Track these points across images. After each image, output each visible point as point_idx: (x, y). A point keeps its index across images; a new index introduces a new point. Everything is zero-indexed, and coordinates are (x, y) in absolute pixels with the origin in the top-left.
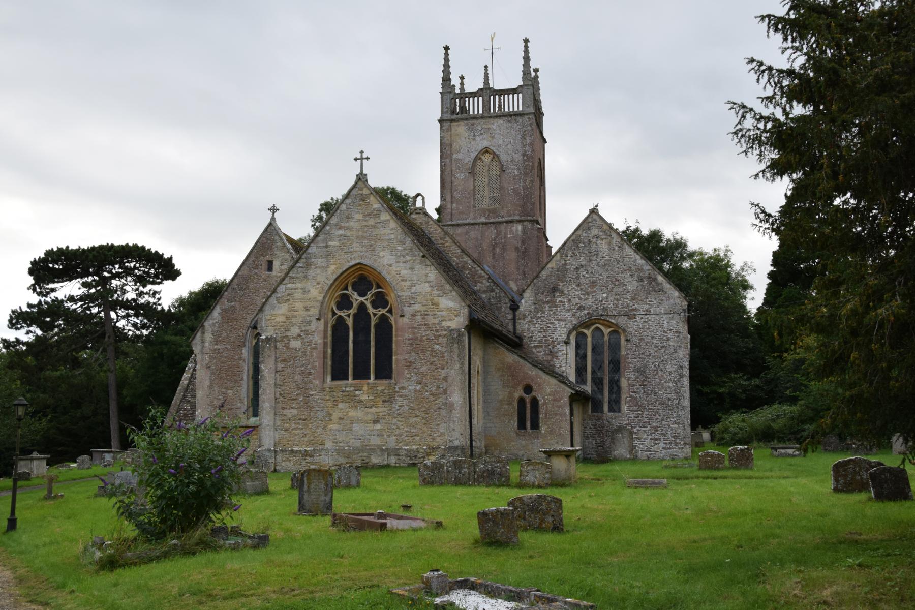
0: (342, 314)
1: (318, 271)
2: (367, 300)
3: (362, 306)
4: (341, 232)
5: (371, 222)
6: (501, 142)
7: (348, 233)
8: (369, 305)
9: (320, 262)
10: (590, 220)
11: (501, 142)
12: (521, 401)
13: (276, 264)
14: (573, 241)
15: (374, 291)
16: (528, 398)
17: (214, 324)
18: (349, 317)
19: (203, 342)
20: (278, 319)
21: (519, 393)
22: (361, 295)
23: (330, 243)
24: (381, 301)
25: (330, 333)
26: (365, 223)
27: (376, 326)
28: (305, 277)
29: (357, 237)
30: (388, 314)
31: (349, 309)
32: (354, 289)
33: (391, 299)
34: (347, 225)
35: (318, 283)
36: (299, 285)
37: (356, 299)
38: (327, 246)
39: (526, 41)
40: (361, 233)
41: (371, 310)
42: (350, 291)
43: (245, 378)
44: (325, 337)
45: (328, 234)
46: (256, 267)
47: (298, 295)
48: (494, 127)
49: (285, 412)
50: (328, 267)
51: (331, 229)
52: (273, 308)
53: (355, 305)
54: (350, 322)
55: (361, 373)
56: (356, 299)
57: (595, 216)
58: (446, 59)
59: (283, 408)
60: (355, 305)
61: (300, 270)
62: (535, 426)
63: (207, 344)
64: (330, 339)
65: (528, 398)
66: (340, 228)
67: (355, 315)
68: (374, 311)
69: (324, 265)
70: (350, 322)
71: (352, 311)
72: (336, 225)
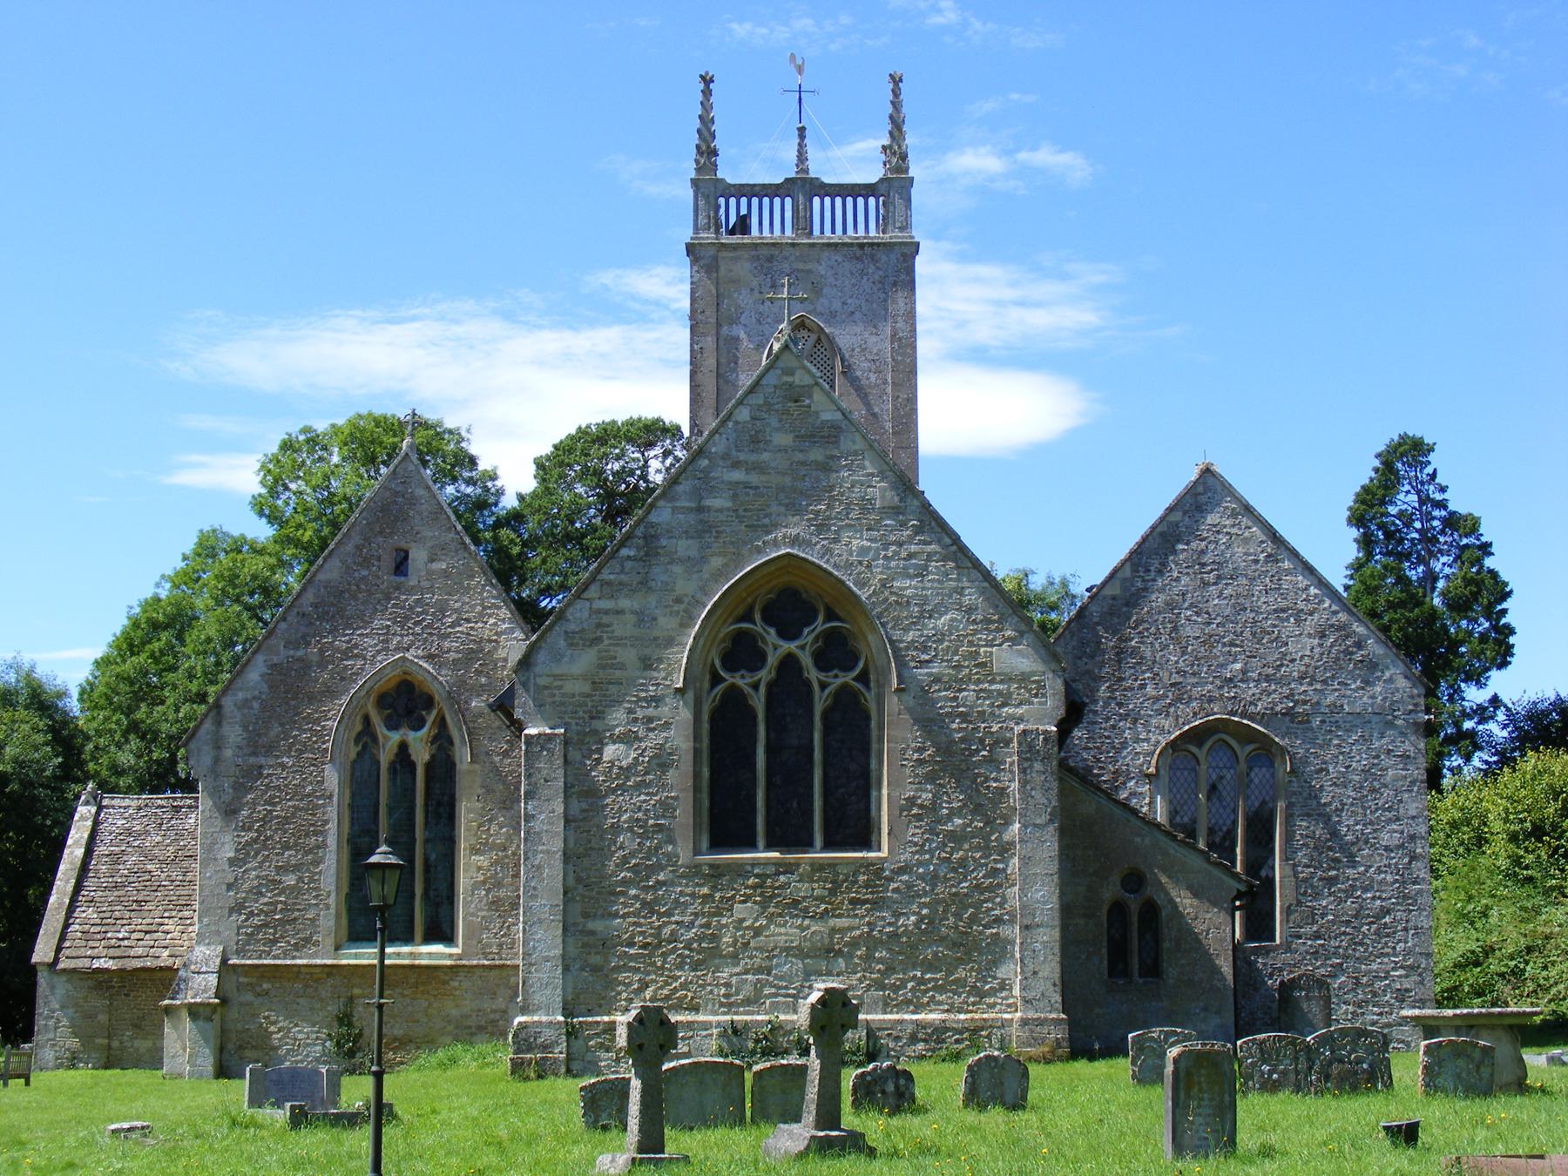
0: (740, 682)
1: (677, 569)
2: (802, 648)
3: (789, 662)
4: (738, 475)
5: (816, 455)
6: (837, 305)
7: (754, 479)
8: (806, 660)
9: (685, 547)
10: (1200, 489)
11: (837, 305)
12: (1118, 909)
13: (418, 556)
14: (1162, 534)
15: (820, 625)
16: (1134, 904)
17: (246, 703)
18: (755, 686)
19: (218, 745)
20: (569, 687)
21: (1110, 891)
22: (786, 635)
23: (707, 503)
24: (838, 650)
25: (706, 726)
26: (800, 456)
27: (826, 715)
28: (644, 583)
29: (781, 489)
30: (859, 686)
31: (754, 669)
32: (768, 619)
33: (871, 645)
34: (753, 458)
35: (678, 601)
36: (624, 603)
37: (776, 647)
38: (700, 509)
39: (896, 81)
40: (788, 480)
41: (813, 675)
42: (758, 626)
43: (332, 841)
44: (697, 737)
45: (705, 477)
46: (366, 562)
47: (623, 627)
48: (822, 269)
49: (591, 925)
50: (703, 560)
51: (712, 466)
52: (557, 657)
53: (772, 660)
54: (759, 702)
55: (790, 835)
56: (776, 647)
57: (1211, 481)
58: (706, 105)
59: (586, 915)
60: (772, 660)
61: (629, 564)
62: (1153, 970)
63: (228, 753)
64: (706, 742)
65: (1134, 904)
66: (736, 465)
67: (771, 686)
68: (822, 676)
69: (693, 553)
70: (759, 702)
71: (765, 675)
72: (726, 456)
